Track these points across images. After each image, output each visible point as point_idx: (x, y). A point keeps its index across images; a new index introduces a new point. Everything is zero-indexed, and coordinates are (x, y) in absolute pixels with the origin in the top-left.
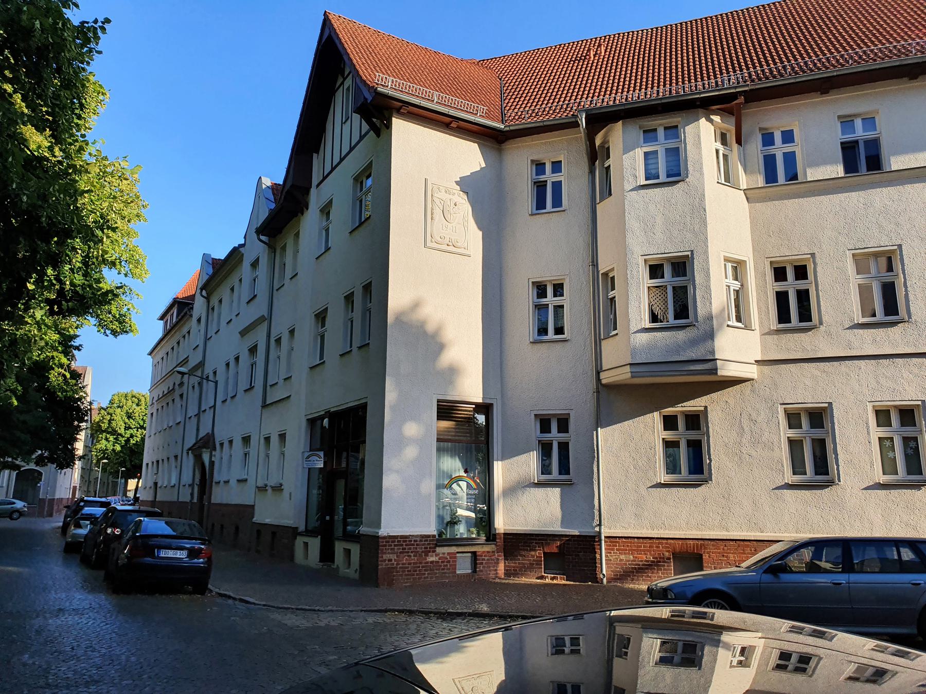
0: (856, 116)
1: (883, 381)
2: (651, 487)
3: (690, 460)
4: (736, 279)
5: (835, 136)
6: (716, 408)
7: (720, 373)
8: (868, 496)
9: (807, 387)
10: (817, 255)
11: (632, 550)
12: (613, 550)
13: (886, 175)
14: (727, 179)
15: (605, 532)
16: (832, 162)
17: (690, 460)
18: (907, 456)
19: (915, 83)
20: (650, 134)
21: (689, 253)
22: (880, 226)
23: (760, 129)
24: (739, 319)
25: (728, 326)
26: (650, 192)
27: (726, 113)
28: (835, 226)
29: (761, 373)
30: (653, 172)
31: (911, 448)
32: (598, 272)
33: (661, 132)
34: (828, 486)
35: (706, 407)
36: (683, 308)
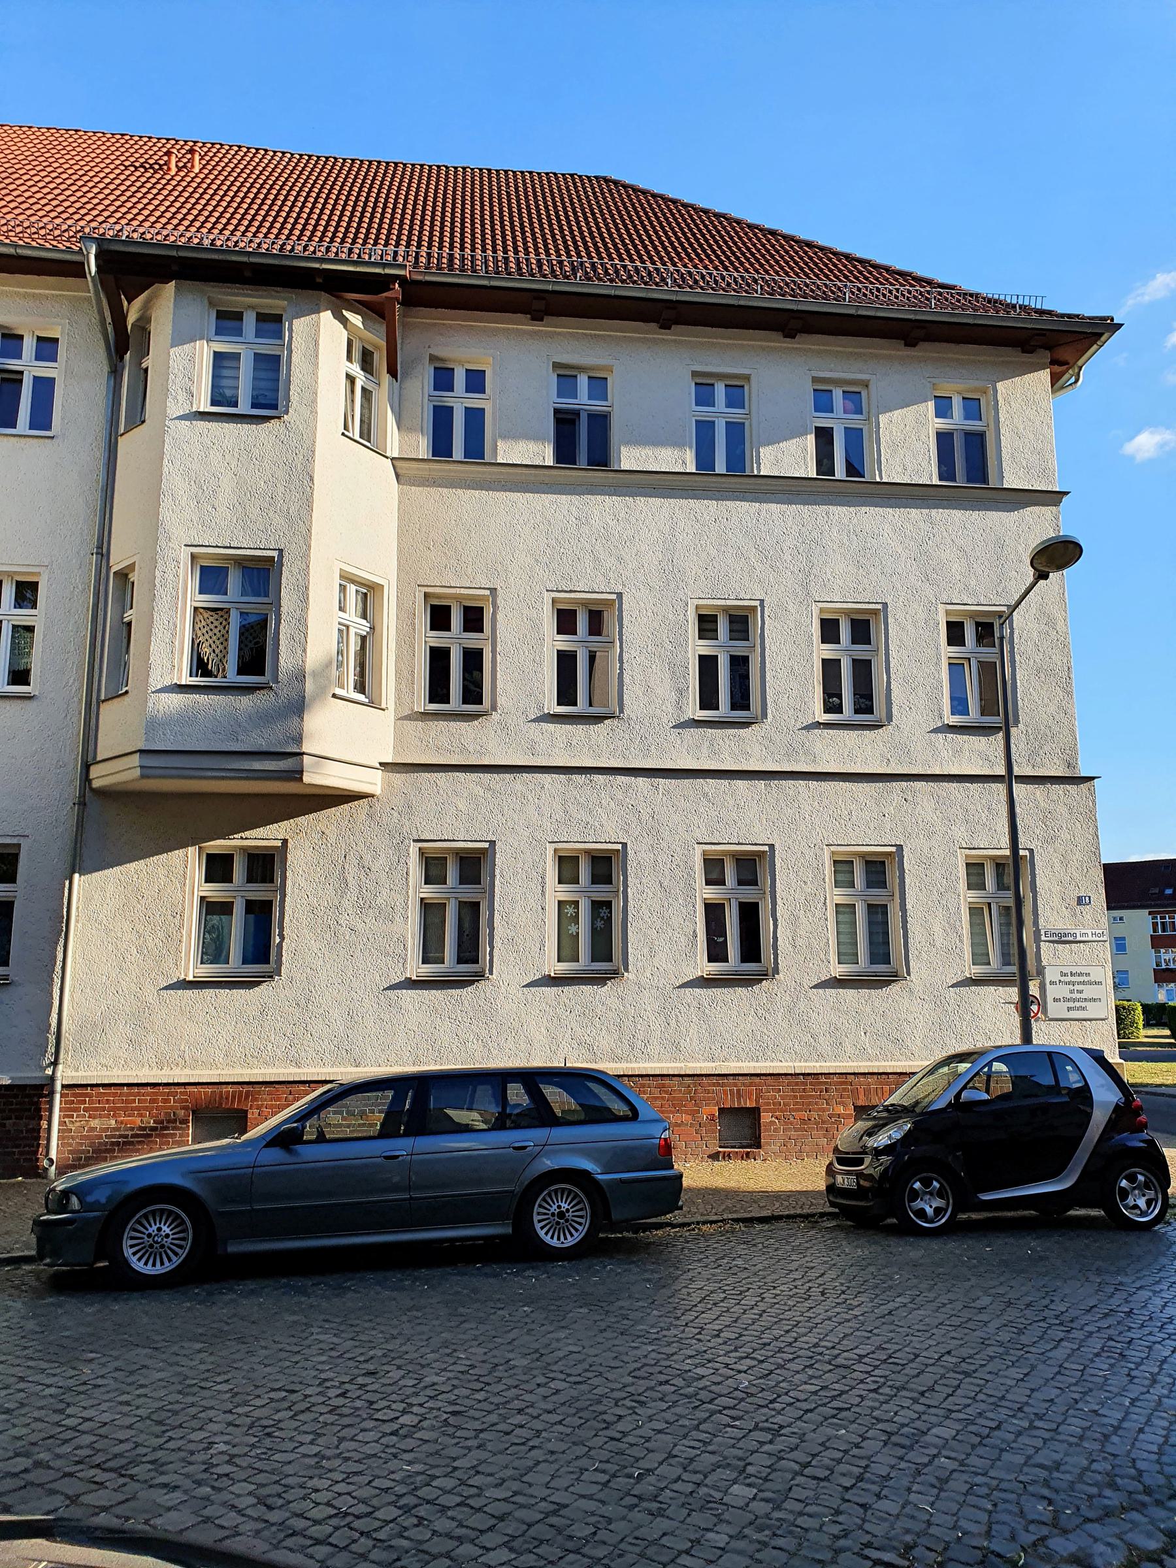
0: (581, 369)
1: (572, 809)
2: (166, 988)
3: (246, 937)
4: (364, 617)
5: (545, 398)
6: (303, 842)
7: (307, 779)
8: (530, 997)
9: (456, 815)
10: (500, 592)
11: (114, 1109)
12: (77, 1110)
13: (611, 475)
14: (366, 433)
15: (65, 1074)
16: (537, 438)
17: (246, 937)
18: (594, 930)
19: (666, 335)
20: (228, 321)
21: (275, 554)
22: (596, 559)
23: (433, 358)
24: (361, 687)
25: (334, 696)
26: (214, 426)
27: (376, 312)
28: (529, 546)
29: (388, 785)
30: (228, 393)
31: (602, 918)
32: (109, 568)
33: (250, 320)
34: (472, 983)
35: (285, 841)
36: (255, 652)
